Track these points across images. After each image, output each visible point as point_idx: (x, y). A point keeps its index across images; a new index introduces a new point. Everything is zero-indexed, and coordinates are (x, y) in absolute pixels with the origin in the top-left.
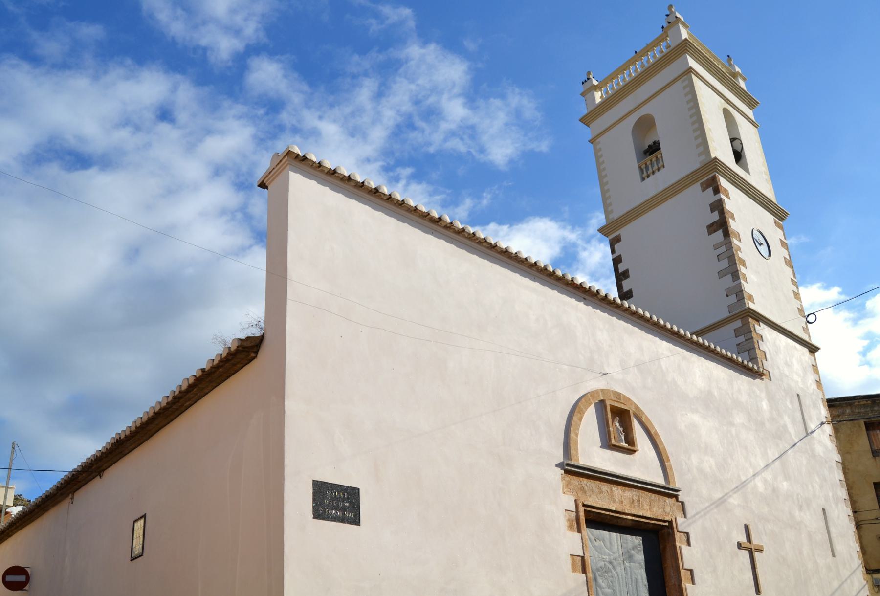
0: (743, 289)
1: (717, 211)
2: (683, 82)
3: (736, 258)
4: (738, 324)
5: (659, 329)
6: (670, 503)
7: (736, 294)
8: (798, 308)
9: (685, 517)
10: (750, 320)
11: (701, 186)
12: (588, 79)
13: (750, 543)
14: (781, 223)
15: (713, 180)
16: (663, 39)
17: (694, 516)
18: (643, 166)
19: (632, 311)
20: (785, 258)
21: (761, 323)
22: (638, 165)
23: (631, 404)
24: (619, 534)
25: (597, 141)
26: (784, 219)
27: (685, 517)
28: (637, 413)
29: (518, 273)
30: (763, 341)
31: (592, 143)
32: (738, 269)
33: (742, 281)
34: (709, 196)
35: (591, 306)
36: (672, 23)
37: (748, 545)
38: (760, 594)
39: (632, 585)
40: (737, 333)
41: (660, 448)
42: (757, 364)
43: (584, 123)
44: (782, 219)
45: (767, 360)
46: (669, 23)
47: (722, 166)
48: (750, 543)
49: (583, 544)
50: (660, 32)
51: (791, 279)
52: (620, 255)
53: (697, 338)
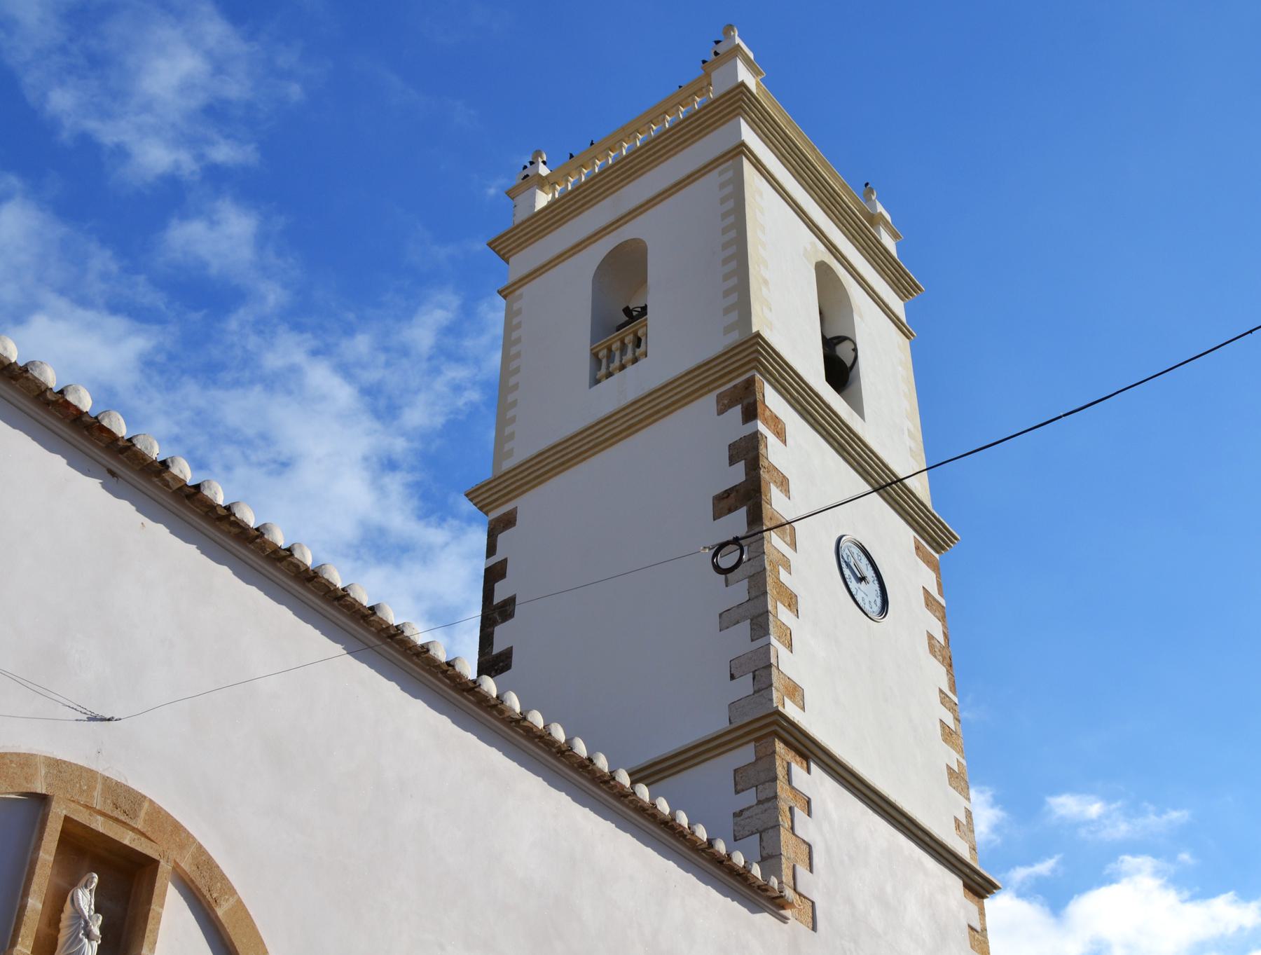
0: (773, 660)
1: (743, 462)
2: (721, 174)
3: (769, 580)
4: (745, 754)
5: (409, 658)
7: (754, 672)
8: (949, 768)
10: (780, 747)
11: (718, 402)
12: (532, 163)
14: (937, 556)
15: (746, 388)
16: (701, 89)
18: (602, 354)
19: (297, 566)
20: (931, 637)
22: (592, 350)
23: (182, 847)
25: (518, 293)
26: (943, 548)
28: (201, 883)
29: (449, 717)
30: (809, 814)
31: (505, 297)
32: (770, 608)
33: (774, 641)
34: (732, 425)
35: (167, 526)
36: (724, 56)
40: (741, 780)
42: (778, 874)
43: (498, 253)
44: (939, 548)
46: (716, 54)
47: (774, 359)
50: (698, 71)
51: (941, 691)
52: (505, 560)
53: (633, 783)
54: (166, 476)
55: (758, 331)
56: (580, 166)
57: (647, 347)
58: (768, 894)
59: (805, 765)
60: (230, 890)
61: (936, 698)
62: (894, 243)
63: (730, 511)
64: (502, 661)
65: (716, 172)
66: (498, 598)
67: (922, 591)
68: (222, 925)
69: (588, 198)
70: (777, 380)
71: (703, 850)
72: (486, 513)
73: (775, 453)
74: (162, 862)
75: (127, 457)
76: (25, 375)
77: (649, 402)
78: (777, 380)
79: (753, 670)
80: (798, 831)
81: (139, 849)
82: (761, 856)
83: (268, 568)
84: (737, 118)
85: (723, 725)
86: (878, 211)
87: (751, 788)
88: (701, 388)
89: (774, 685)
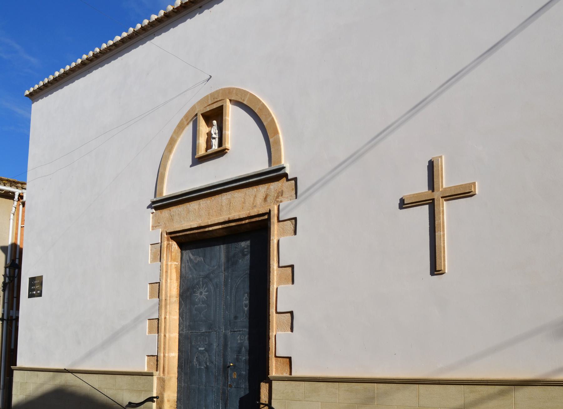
24: (222, 246)
48: (433, 191)
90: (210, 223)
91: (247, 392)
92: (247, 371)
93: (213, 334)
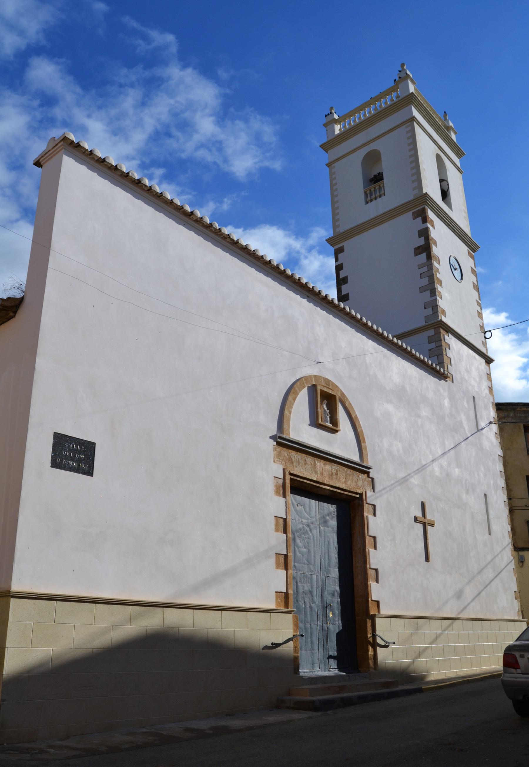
0: (438, 304)
1: (423, 237)
2: (406, 127)
4: (431, 332)
6: (362, 478)
7: (432, 307)
8: (480, 325)
9: (374, 491)
10: (442, 330)
13: (425, 518)
14: (473, 254)
16: (395, 90)
17: (381, 490)
18: (368, 192)
19: (346, 312)
21: (449, 334)
22: (364, 191)
23: (338, 391)
24: (317, 502)
25: (333, 165)
26: (475, 251)
27: (374, 491)
28: (342, 399)
31: (328, 167)
32: (436, 287)
33: (438, 298)
36: (403, 78)
37: (422, 519)
38: (428, 562)
39: (324, 546)
40: (430, 340)
41: (358, 430)
44: (474, 251)
45: (452, 365)
46: (400, 78)
47: (431, 201)
48: (425, 518)
49: (286, 507)
50: (392, 84)
51: (477, 301)
54: (320, 296)
55: (427, 192)
56: (349, 116)
57: (384, 191)
58: (444, 375)
59: (447, 334)
60: (347, 399)
61: (476, 303)
62: (455, 136)
63: (420, 254)
64: (346, 297)
65: (405, 126)
66: (341, 277)
67: (470, 268)
68: (347, 408)
69: (356, 131)
70: (431, 207)
71: (430, 366)
72: (333, 247)
73: (434, 233)
74: (337, 396)
75: (311, 292)
76: (292, 277)
77: (389, 213)
78: (431, 207)
79: (432, 306)
80: (448, 355)
81: (333, 394)
82: (438, 363)
83: (339, 313)
84: (411, 105)
85: (423, 324)
86: (450, 125)
87: (433, 342)
88: (407, 210)
89: (439, 311)
90: (326, 482)
91: (341, 628)
92: (340, 611)
93: (314, 577)
